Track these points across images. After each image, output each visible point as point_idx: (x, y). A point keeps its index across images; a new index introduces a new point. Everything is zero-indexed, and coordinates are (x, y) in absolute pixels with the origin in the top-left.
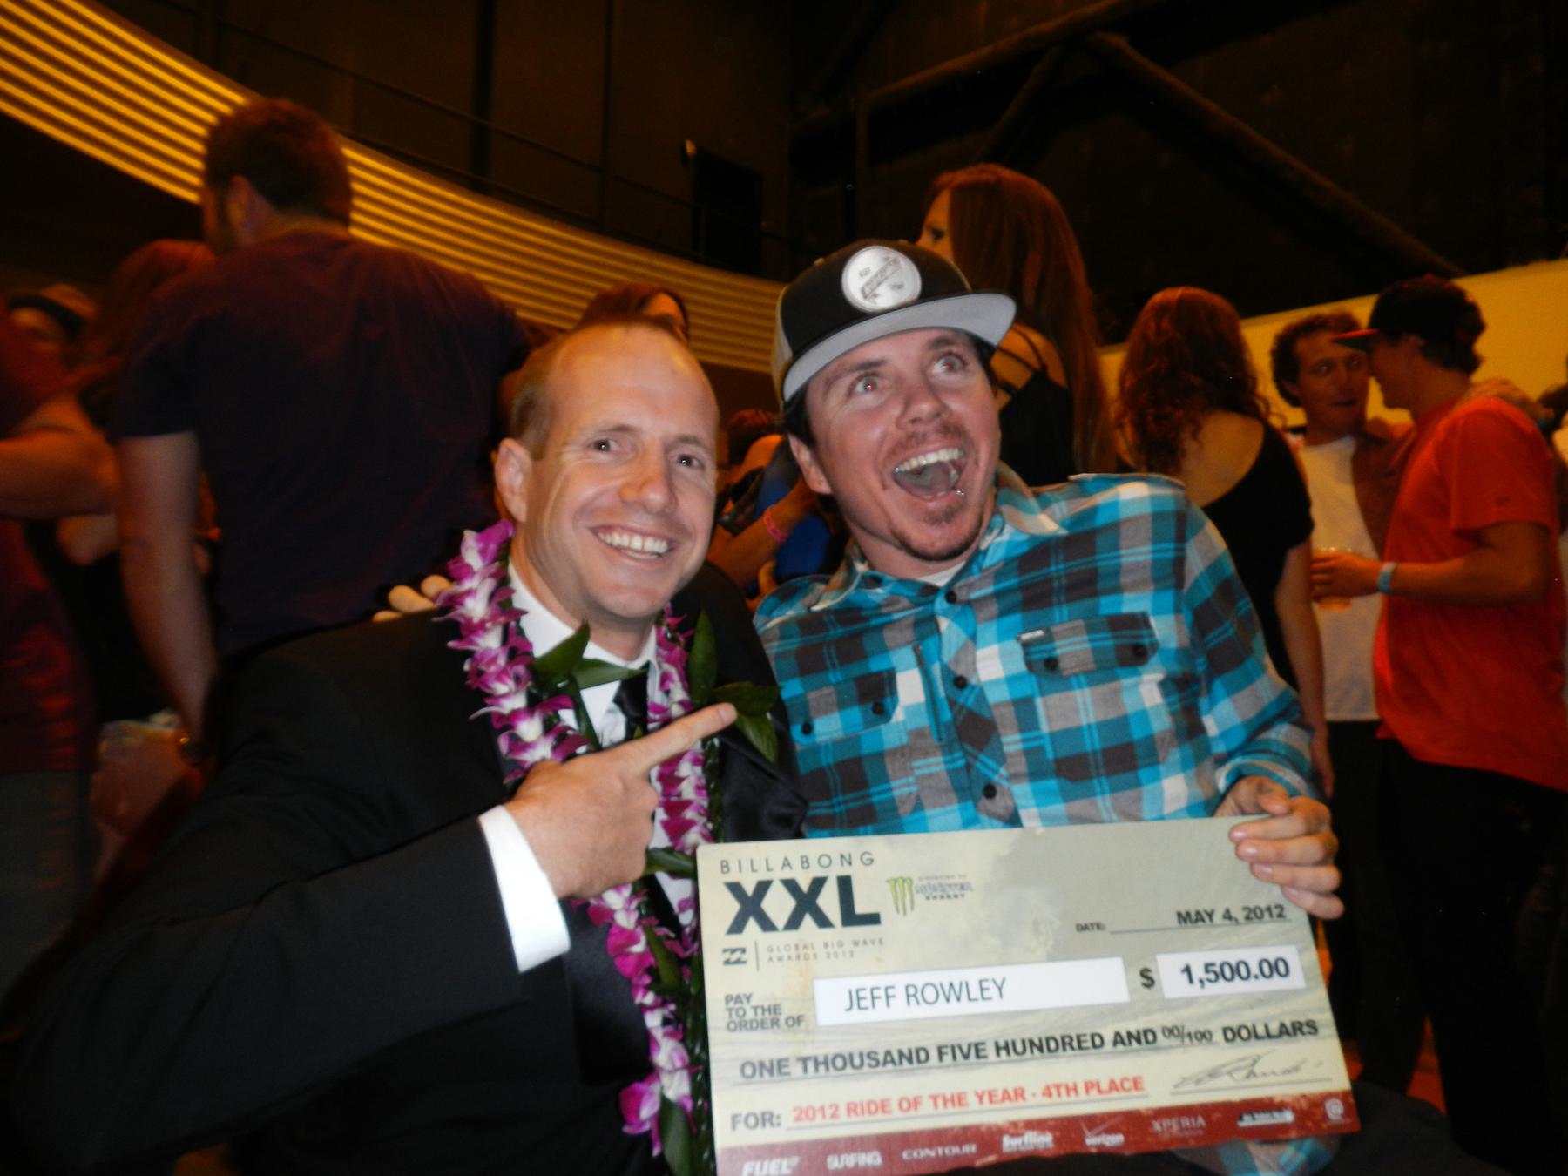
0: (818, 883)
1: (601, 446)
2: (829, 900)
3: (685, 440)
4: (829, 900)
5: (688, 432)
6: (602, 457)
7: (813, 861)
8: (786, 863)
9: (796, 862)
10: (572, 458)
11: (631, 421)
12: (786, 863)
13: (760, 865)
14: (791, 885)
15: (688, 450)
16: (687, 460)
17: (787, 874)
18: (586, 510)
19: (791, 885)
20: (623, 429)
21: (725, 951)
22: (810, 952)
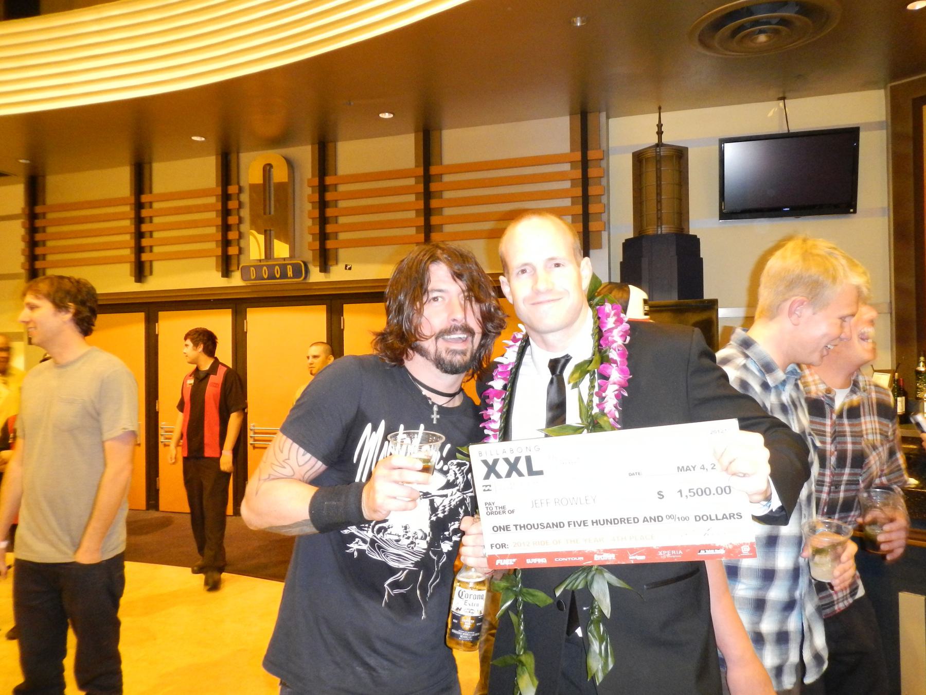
1: (523, 271)
12: (504, 452)
18: (525, 300)
20: (526, 264)
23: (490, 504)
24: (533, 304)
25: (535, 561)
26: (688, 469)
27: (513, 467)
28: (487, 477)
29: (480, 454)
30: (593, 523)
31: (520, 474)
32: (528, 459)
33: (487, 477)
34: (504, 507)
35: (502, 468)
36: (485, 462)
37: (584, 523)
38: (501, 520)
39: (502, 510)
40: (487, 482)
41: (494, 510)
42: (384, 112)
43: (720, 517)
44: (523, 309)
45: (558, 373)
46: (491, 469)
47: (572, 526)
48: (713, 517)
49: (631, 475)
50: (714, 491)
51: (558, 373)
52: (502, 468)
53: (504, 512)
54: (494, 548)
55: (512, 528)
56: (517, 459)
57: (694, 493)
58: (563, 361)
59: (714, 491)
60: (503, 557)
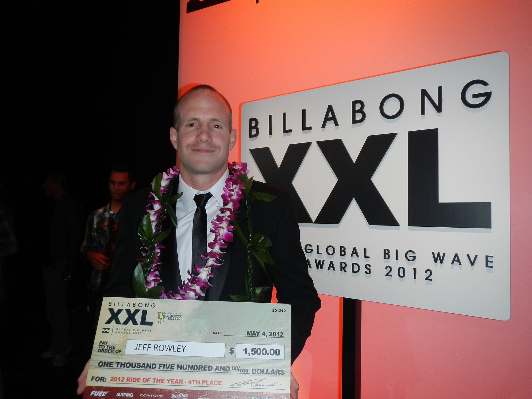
0: (377, 146)
1: (191, 125)
2: (392, 179)
3: (214, 120)
4: (392, 179)
5: (214, 118)
6: (192, 128)
7: (137, 305)
8: (129, 305)
9: (131, 305)
10: (183, 129)
11: (197, 116)
12: (129, 305)
13: (121, 305)
14: (333, 150)
15: (217, 123)
16: (217, 126)
17: (128, 308)
18: (188, 146)
19: (128, 311)
20: (195, 119)
21: (492, 267)
22: (362, 261)
23: (103, 343)
24: (194, 150)
25: (123, 394)
26: (254, 333)
27: (131, 317)
28: (109, 322)
29: (110, 304)
30: (178, 367)
31: (135, 323)
32: (145, 312)
33: (109, 322)
34: (114, 347)
35: (123, 316)
36: (111, 310)
37: (172, 366)
38: (107, 357)
39: (112, 349)
40: (107, 326)
41: (106, 348)
42: (130, 398)
43: (270, 371)
44: (185, 153)
45: (202, 205)
46: (114, 316)
47: (162, 368)
48: (265, 371)
49: (214, 333)
50: (268, 352)
51: (202, 205)
52: (123, 316)
53: (112, 351)
54: (94, 380)
55: (115, 365)
56: (137, 311)
57: (255, 351)
58: (205, 196)
59: (268, 352)
60: (99, 389)
